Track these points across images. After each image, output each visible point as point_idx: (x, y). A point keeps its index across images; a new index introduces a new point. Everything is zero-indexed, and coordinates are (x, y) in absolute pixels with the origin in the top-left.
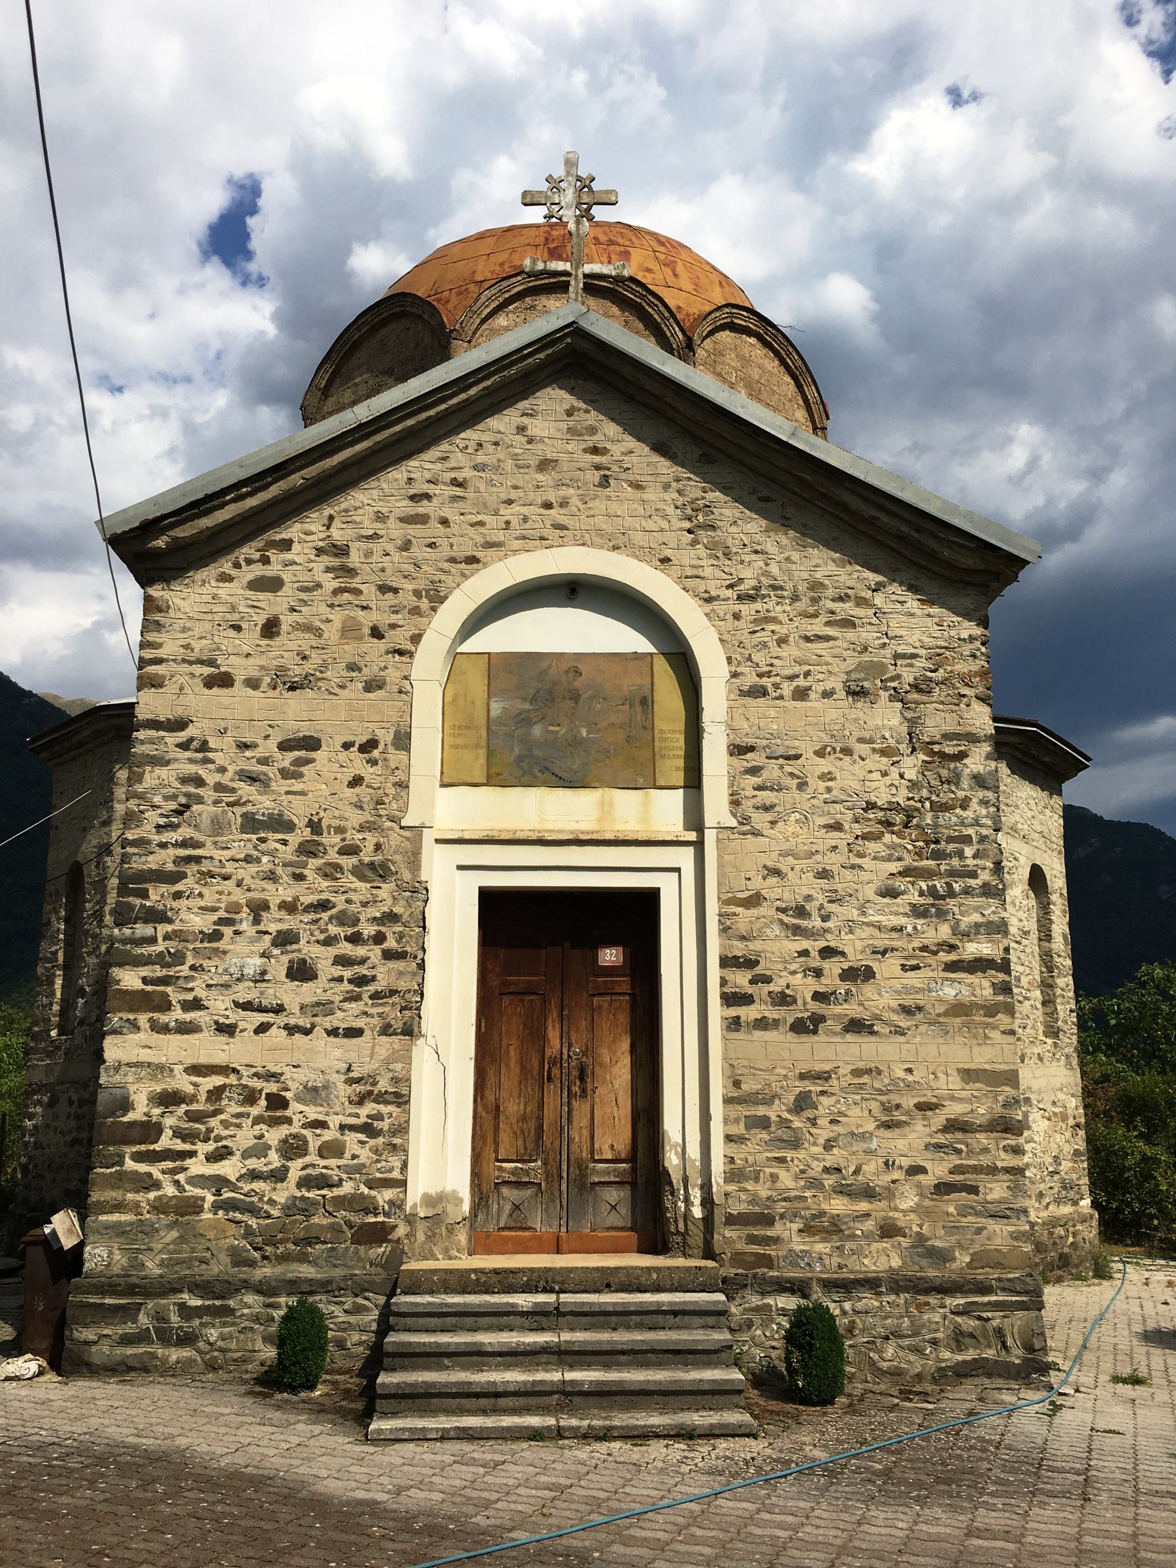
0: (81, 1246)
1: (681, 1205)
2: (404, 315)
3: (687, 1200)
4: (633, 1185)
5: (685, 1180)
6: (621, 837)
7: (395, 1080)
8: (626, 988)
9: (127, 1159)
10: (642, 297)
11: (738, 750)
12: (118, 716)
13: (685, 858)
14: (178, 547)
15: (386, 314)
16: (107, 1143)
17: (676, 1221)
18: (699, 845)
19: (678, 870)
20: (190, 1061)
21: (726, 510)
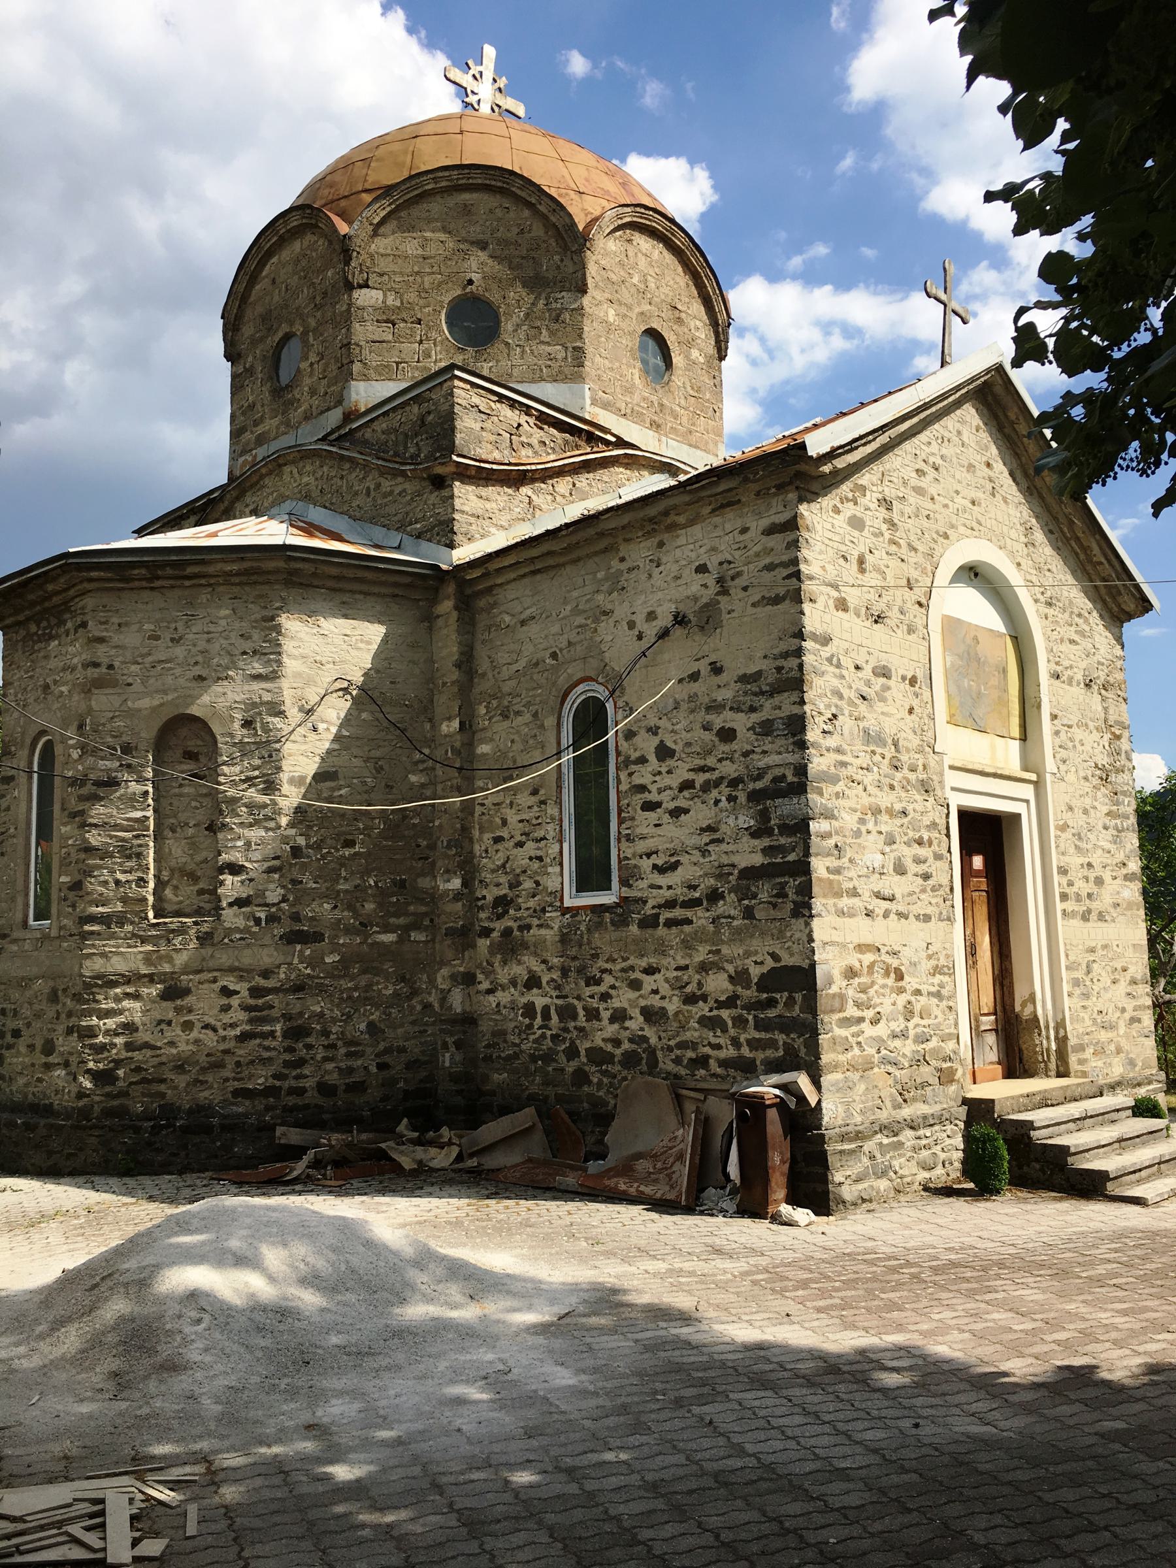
0: (819, 1102)
1: (1045, 1042)
2: (502, 191)
3: (1048, 1038)
4: (996, 1031)
5: (1047, 1027)
6: (999, 772)
7: (947, 956)
8: (984, 887)
9: (835, 1027)
10: (702, 267)
11: (1054, 717)
12: (304, 559)
13: (1028, 792)
14: (835, 472)
15: (480, 181)
16: (825, 1013)
17: (1042, 1054)
18: (1038, 785)
19: (1027, 801)
20: (856, 941)
21: (1039, 536)
